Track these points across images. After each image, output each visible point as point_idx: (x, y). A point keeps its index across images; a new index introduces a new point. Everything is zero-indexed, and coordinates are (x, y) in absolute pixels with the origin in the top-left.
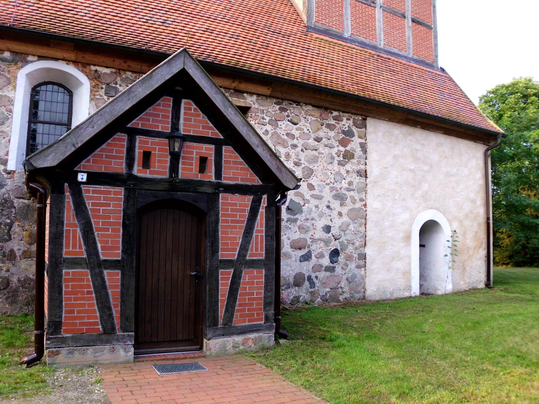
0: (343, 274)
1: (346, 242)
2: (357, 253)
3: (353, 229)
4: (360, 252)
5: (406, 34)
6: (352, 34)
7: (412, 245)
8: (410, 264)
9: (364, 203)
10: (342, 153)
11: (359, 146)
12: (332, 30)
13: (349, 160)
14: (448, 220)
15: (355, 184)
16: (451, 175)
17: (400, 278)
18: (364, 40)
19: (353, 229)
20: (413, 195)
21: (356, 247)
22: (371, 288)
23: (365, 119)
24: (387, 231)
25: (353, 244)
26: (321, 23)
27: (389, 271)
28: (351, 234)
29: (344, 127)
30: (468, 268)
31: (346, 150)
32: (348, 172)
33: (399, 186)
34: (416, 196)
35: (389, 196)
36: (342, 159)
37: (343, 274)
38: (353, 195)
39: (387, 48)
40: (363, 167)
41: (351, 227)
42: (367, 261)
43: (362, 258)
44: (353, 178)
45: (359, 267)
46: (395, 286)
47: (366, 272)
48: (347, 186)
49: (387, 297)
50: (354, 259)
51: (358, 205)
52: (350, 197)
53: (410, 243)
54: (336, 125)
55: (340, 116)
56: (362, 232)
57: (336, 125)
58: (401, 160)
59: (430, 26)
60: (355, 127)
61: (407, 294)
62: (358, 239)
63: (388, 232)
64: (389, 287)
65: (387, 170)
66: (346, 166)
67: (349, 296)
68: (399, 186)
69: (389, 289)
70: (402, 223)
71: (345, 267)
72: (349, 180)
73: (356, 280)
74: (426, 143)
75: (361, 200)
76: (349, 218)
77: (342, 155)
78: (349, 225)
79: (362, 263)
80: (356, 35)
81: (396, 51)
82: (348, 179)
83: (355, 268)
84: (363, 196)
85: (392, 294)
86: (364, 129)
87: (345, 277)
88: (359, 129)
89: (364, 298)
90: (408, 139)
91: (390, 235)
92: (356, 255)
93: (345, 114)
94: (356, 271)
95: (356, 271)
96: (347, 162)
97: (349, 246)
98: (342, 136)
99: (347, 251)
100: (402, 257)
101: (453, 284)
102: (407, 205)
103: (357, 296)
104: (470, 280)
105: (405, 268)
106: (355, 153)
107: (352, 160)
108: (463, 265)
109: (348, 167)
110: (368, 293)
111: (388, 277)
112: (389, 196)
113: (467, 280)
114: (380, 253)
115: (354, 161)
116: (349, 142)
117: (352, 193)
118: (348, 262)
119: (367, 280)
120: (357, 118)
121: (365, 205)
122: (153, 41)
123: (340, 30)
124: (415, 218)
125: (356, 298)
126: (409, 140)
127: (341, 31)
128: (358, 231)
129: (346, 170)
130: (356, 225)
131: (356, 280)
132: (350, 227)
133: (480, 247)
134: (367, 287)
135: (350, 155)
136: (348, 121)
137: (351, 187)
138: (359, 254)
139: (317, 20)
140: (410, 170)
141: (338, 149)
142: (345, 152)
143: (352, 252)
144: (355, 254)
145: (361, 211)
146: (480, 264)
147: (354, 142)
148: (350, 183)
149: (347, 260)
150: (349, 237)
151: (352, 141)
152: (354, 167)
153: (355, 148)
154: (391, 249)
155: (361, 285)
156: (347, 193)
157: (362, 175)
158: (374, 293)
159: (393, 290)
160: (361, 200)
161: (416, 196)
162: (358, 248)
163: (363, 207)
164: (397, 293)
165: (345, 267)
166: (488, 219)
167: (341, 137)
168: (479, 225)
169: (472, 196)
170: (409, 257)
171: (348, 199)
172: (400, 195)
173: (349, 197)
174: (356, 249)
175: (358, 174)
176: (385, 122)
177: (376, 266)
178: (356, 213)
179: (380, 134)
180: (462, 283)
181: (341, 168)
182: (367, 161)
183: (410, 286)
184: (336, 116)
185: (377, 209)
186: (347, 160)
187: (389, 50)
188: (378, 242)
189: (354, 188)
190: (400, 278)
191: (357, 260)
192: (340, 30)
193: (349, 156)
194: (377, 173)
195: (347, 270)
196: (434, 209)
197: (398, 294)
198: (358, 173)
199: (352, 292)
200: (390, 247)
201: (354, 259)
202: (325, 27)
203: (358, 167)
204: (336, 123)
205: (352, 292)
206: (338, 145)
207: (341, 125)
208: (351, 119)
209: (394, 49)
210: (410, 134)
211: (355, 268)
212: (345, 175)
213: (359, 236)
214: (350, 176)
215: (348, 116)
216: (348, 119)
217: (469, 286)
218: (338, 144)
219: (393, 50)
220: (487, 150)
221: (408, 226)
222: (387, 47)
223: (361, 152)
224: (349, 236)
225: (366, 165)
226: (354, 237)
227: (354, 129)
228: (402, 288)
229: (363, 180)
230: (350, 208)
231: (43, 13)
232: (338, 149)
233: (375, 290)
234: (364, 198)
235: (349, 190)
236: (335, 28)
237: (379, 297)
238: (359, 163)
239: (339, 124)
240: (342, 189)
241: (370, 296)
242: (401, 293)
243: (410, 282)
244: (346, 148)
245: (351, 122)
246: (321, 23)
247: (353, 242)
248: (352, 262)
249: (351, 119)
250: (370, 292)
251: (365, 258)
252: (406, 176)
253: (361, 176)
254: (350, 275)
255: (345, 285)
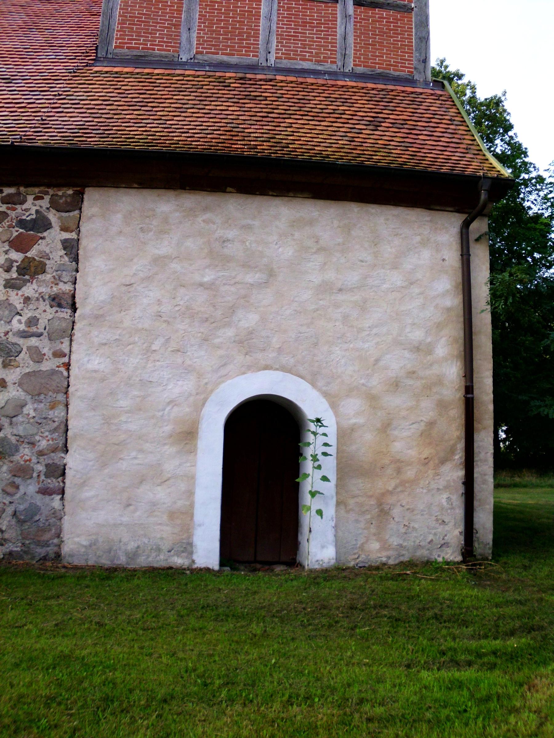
0: (7, 502)
1: (13, 439)
2: (44, 463)
3: (32, 414)
4: (50, 462)
5: (338, 30)
6: (197, 53)
7: (199, 451)
8: (190, 494)
9: (66, 360)
10: (15, 264)
11: (60, 246)
12: (151, 55)
13: (32, 277)
14: (326, 395)
15: (42, 323)
16: (340, 290)
17: (160, 524)
18: (225, 58)
19: (32, 414)
20: (206, 340)
21: (41, 451)
22: (77, 539)
23: (82, 193)
24: (123, 418)
25: (32, 444)
26: (128, 48)
27: (129, 505)
28: (28, 423)
29: (27, 214)
30: (396, 512)
31: (26, 257)
32: (27, 300)
33: (165, 321)
34: (217, 341)
35: (134, 343)
36: (15, 275)
37: (7, 502)
38: (37, 344)
39: (285, 63)
40: (67, 288)
41: (29, 409)
42: (67, 481)
43: (56, 474)
44: (38, 311)
45: (45, 492)
46: (146, 541)
47: (66, 503)
48: (22, 327)
49: (117, 562)
50: (35, 475)
51: (47, 365)
52: (29, 348)
53: (196, 446)
54: (9, 212)
55: (19, 194)
56: (56, 419)
57: (9, 212)
58: (175, 266)
59: (405, 6)
60: (54, 211)
61: (179, 561)
62: (47, 434)
63: (126, 422)
64: (124, 540)
65: (131, 290)
66: (24, 289)
67: (19, 549)
68: (165, 321)
69: (125, 544)
70: (172, 402)
71: (10, 490)
72: (29, 315)
73: (37, 518)
74: (257, 223)
75: (59, 354)
76: (24, 391)
77: (15, 269)
78: (23, 406)
79: (53, 483)
80: (207, 53)
81: (306, 65)
82: (28, 314)
83: (38, 492)
84: (65, 347)
85: (134, 555)
86: (77, 212)
87: (10, 510)
88: (64, 214)
89: (58, 555)
90: (200, 219)
91: (132, 427)
92: (40, 468)
93: (30, 189)
94: (39, 500)
95: (39, 500)
96: (26, 282)
97: (21, 448)
98: (17, 231)
99: (17, 458)
100: (168, 479)
101: (336, 546)
102: (188, 362)
103: (41, 551)
104: (404, 540)
105: (175, 503)
106: (47, 262)
107: (40, 276)
108: (380, 504)
109: (29, 290)
110: (66, 549)
111: (125, 519)
112: (134, 343)
113: (395, 541)
114: (104, 465)
115: (48, 277)
116: (34, 241)
117: (33, 341)
118: (18, 480)
119: (67, 523)
120: (60, 193)
121: (67, 366)
122: (299, 132)
123: (169, 51)
124: (212, 391)
125: (37, 554)
126: (204, 221)
127: (171, 53)
128: (45, 418)
129: (22, 296)
130: (42, 405)
131: (37, 518)
132: (25, 410)
133: (443, 462)
134: (66, 536)
135: (36, 267)
136: (38, 202)
137: (34, 329)
138: (47, 466)
139: (120, 43)
140: (201, 285)
141: (6, 256)
142: (22, 262)
143: (30, 460)
144: (39, 465)
145: (55, 377)
146: (444, 502)
147: (47, 239)
148: (32, 322)
149: (15, 476)
150: (20, 430)
151: (42, 238)
152: (43, 289)
153: (48, 251)
154: (135, 458)
155: (50, 530)
156: (21, 341)
157: (63, 303)
158: (83, 550)
159: (138, 547)
160: (59, 354)
161: (217, 341)
162: (46, 451)
163: (62, 369)
164: (148, 556)
165: (10, 490)
166: (469, 389)
167: (15, 234)
168: (442, 405)
169: (417, 335)
170: (191, 479)
171: (22, 355)
172: (168, 340)
173: (25, 349)
174: (41, 453)
175: (53, 303)
176: (132, 191)
177: (92, 493)
178: (43, 381)
179: (118, 218)
180: (375, 545)
181: (12, 293)
182: (78, 275)
183: (191, 544)
184: (9, 195)
185: (95, 371)
186: (27, 277)
187: (289, 66)
188: (99, 443)
189: (41, 330)
190: (160, 524)
191: (42, 477)
192: (169, 51)
193: (33, 269)
194: (102, 298)
195: (17, 496)
196: (277, 369)
197: (150, 559)
198: (54, 299)
199: (27, 542)
200: (134, 454)
201: (35, 475)
202: (135, 52)
203: (55, 289)
204: (8, 208)
205: (27, 542)
206: (8, 250)
207: (19, 210)
208: (45, 197)
209: (301, 62)
210: (206, 209)
211: (38, 492)
212: (19, 307)
213: (47, 427)
214: (31, 306)
215: (40, 192)
216: (37, 198)
217: (400, 555)
218: (7, 248)
219: (299, 64)
220: (466, 225)
221: (187, 410)
222: (285, 61)
223: (66, 259)
224: (21, 428)
225: (75, 283)
226: (35, 431)
227: (53, 217)
228: (165, 547)
229: (66, 313)
230: (27, 370)
231: (173, 126)
232: (6, 256)
233: (85, 543)
234: (67, 351)
235: (25, 335)
236: (158, 50)
237: (94, 559)
238: (57, 280)
239: (15, 209)
240: (10, 333)
241: (71, 556)
242: (162, 557)
243: (190, 536)
244: (27, 255)
245: (45, 203)
246: (128, 48)
247: (32, 440)
248: (29, 481)
249: (45, 197)
250: (71, 547)
251: (63, 474)
252: (186, 298)
253: (60, 305)
254: (22, 507)
255: (9, 526)
